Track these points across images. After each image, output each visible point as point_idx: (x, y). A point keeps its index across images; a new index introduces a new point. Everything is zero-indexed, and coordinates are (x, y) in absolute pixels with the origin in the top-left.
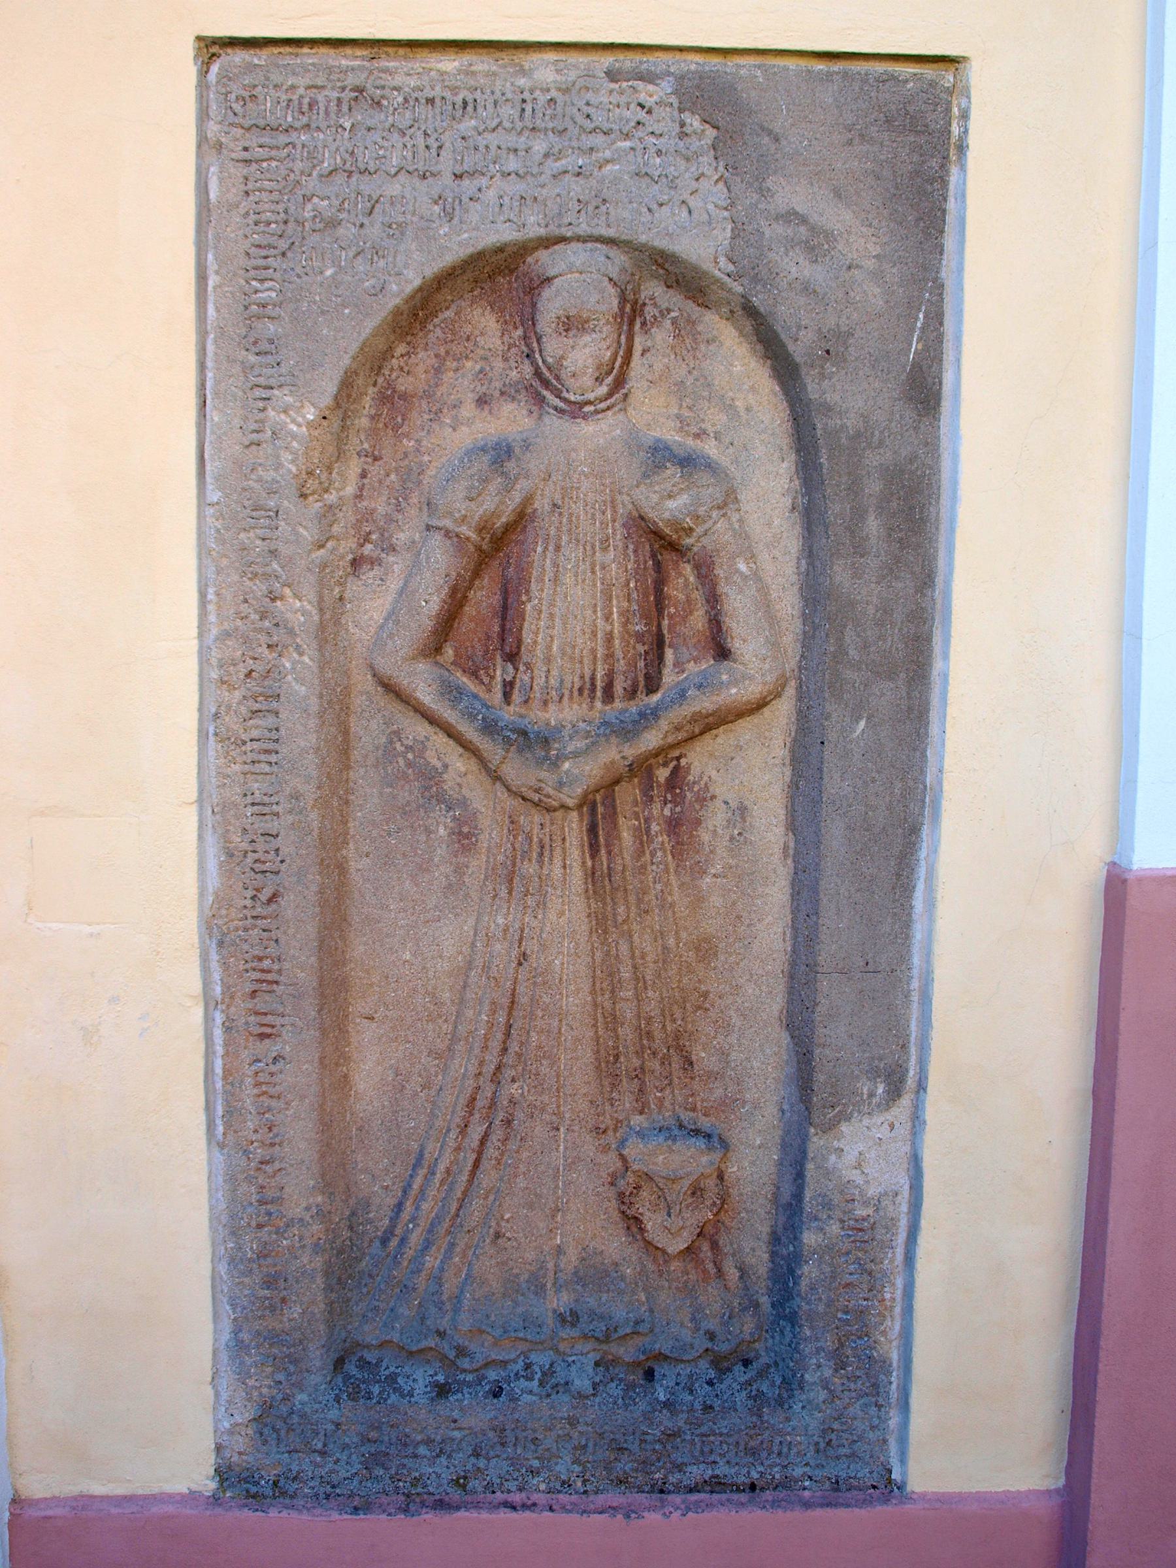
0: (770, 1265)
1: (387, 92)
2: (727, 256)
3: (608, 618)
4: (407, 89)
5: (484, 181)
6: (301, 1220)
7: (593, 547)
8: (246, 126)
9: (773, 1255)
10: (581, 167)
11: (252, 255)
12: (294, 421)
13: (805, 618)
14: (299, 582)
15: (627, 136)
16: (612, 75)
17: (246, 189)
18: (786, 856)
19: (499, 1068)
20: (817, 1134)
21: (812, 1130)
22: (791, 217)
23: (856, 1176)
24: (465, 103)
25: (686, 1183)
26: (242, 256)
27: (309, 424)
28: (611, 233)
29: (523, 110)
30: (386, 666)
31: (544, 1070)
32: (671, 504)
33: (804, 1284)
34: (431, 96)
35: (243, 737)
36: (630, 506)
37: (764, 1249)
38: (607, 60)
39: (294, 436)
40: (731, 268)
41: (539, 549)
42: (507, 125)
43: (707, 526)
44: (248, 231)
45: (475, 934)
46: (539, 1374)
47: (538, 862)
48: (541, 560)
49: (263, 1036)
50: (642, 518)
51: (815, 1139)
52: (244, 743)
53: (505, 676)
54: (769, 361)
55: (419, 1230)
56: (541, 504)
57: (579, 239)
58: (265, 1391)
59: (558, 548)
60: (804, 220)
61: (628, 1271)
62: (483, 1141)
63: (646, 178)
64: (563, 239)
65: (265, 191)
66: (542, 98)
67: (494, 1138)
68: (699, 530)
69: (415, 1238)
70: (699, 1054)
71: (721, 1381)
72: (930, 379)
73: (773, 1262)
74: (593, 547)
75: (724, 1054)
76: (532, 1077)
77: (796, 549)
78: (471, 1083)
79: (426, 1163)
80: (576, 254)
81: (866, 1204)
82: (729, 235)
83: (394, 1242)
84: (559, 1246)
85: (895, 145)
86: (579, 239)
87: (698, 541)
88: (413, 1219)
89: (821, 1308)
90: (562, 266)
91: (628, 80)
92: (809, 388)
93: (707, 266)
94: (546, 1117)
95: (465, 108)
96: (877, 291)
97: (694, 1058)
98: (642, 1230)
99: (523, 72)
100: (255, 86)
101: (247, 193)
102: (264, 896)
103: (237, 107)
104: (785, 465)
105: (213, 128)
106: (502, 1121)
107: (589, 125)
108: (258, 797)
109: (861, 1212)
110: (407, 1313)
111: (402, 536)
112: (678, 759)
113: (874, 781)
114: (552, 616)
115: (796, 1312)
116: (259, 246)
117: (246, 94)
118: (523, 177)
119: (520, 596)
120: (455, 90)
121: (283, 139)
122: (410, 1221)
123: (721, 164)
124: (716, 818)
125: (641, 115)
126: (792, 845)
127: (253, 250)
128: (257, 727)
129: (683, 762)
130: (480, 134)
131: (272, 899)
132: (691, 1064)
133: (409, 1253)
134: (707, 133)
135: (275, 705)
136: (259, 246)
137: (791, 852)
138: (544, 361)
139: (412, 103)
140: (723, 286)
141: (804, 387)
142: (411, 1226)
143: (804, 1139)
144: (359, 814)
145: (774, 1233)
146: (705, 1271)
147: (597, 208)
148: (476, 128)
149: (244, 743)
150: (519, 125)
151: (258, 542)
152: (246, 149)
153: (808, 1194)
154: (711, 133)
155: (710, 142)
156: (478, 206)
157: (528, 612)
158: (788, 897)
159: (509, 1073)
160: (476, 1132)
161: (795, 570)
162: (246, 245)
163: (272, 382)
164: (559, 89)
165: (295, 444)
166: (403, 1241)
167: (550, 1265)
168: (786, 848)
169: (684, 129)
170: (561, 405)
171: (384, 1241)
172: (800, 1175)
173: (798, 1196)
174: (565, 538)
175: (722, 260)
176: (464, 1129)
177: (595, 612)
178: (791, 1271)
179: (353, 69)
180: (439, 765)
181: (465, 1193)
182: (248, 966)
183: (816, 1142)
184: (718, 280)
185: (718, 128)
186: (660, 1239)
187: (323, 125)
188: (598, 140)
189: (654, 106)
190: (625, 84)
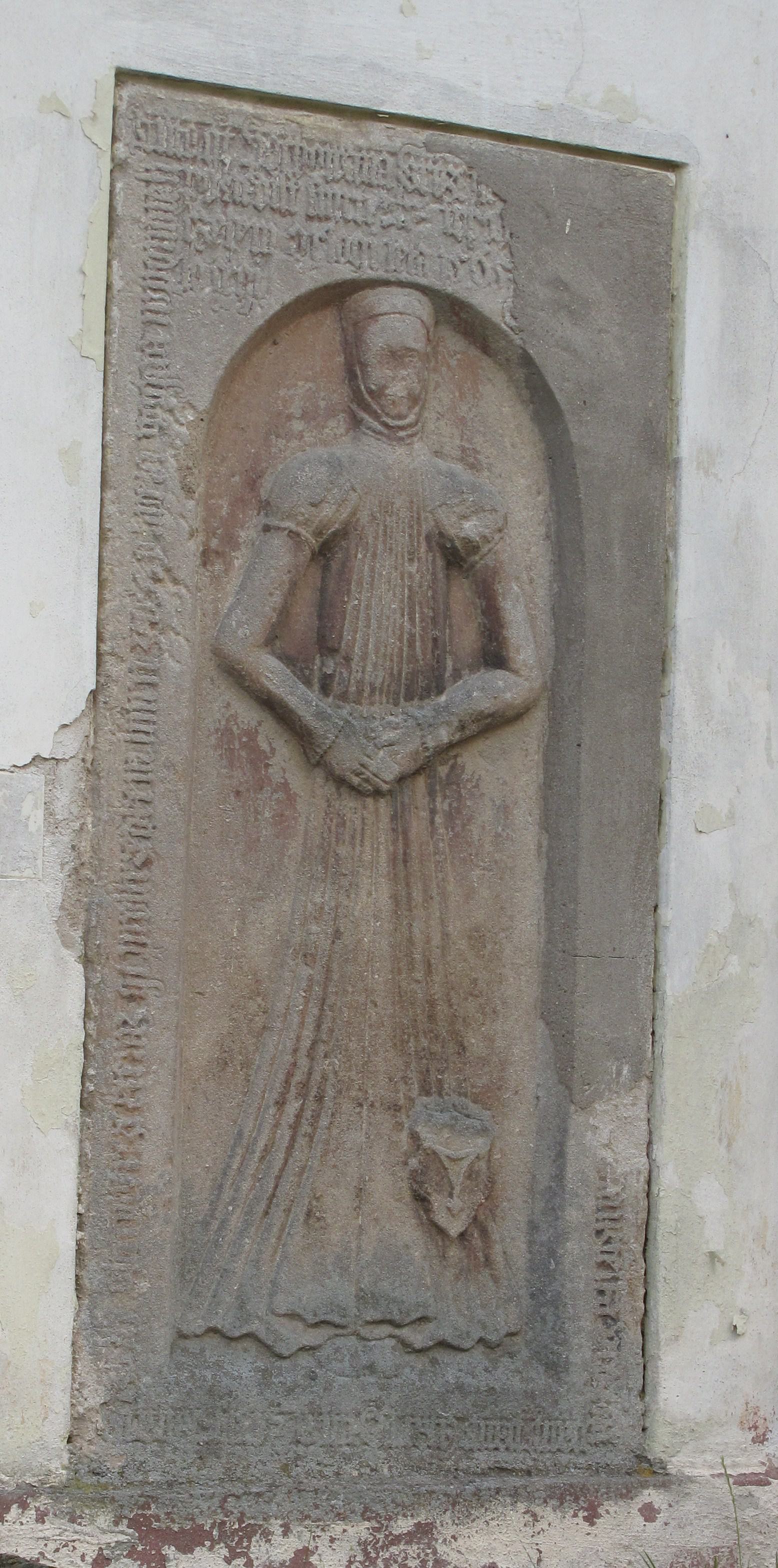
0: (528, 1256)
1: (258, 136)
2: (511, 312)
3: (412, 619)
4: (273, 136)
5: (331, 225)
6: (156, 1187)
7: (403, 556)
8: (148, 150)
9: (531, 1243)
10: (403, 222)
11: (149, 266)
12: (177, 421)
13: (556, 632)
14: (179, 567)
15: (439, 200)
16: (428, 146)
17: (146, 206)
18: (539, 853)
19: (314, 1043)
20: (577, 1111)
21: (573, 1108)
22: (558, 283)
23: (608, 1155)
24: (317, 155)
25: (465, 1164)
26: (141, 265)
27: (189, 425)
28: (423, 281)
29: (361, 166)
30: (233, 648)
31: (353, 1045)
32: (467, 525)
33: (567, 1261)
34: (292, 144)
35: (127, 706)
36: (433, 523)
37: (523, 1239)
38: (424, 135)
39: (178, 435)
40: (513, 323)
41: (360, 556)
42: (349, 178)
43: (490, 546)
44: (146, 244)
45: (293, 912)
46: (348, 1356)
47: (351, 843)
48: (361, 562)
49: (131, 998)
50: (441, 534)
51: (575, 1117)
52: (128, 712)
53: (325, 669)
54: (531, 406)
55: (239, 1210)
56: (364, 517)
57: (401, 284)
58: (112, 1374)
59: (374, 555)
60: (566, 287)
61: (416, 1254)
62: (298, 1117)
63: (451, 238)
64: (386, 283)
65: (161, 210)
66: (378, 159)
67: (308, 1114)
68: (485, 549)
69: (235, 1222)
70: (473, 1040)
71: (495, 1368)
72: (658, 433)
73: (530, 1252)
74: (403, 556)
75: (490, 1040)
76: (343, 1053)
77: (548, 574)
78: (288, 1058)
79: (245, 1142)
80: (400, 298)
81: (615, 1181)
82: (511, 294)
83: (215, 1225)
84: (360, 1226)
85: (633, 230)
86: (401, 284)
87: (481, 559)
88: (233, 1200)
89: (582, 1286)
90: (385, 308)
91: (441, 152)
92: (572, 434)
93: (497, 319)
94: (353, 1093)
95: (317, 158)
96: (619, 353)
97: (466, 1044)
98: (428, 1211)
99: (365, 135)
100: (156, 116)
101: (146, 210)
102: (139, 860)
103: (141, 132)
104: (540, 498)
105: (122, 150)
106: (316, 1097)
107: (410, 187)
108: (135, 765)
109: (612, 1190)
110: (228, 1299)
111: (243, 534)
112: (456, 757)
113: (618, 782)
114: (368, 618)
115: (560, 1292)
116: (155, 259)
117: (149, 122)
118: (359, 226)
119: (343, 597)
120: (310, 142)
121: (176, 166)
122: (229, 1204)
123: (508, 232)
124: (486, 815)
125: (450, 183)
126: (545, 843)
127: (150, 262)
128: (137, 699)
129: (459, 760)
130: (327, 182)
131: (147, 863)
132: (464, 1049)
133: (230, 1236)
134: (497, 203)
135: (154, 679)
136: (155, 259)
137: (544, 850)
138: (367, 388)
139: (277, 149)
140: (506, 336)
141: (566, 431)
142: (231, 1208)
143: (564, 1118)
144: (199, 792)
145: (531, 1222)
146: (476, 1257)
147: (415, 258)
148: (325, 177)
149: (128, 712)
150: (358, 180)
151: (145, 527)
152: (147, 170)
153: (570, 1172)
154: (500, 205)
155: (498, 212)
156: (325, 246)
157: (348, 612)
158: (541, 891)
159: (322, 1048)
160: (293, 1107)
161: (548, 592)
162: (144, 256)
163: (163, 382)
164: (388, 152)
165: (178, 442)
166: (224, 1223)
167: (353, 1245)
168: (540, 846)
169: (481, 199)
170: (380, 428)
171: (206, 1224)
172: (561, 1154)
173: (559, 1177)
174: (380, 547)
175: (508, 318)
176: (281, 1104)
177: (403, 615)
178: (552, 1253)
179: (233, 113)
180: (268, 750)
181: (282, 1170)
182: (121, 928)
183: (577, 1119)
184: (503, 332)
185: (505, 201)
186: (442, 1219)
187: (209, 158)
188: (416, 200)
189: (459, 176)
190: (438, 155)
